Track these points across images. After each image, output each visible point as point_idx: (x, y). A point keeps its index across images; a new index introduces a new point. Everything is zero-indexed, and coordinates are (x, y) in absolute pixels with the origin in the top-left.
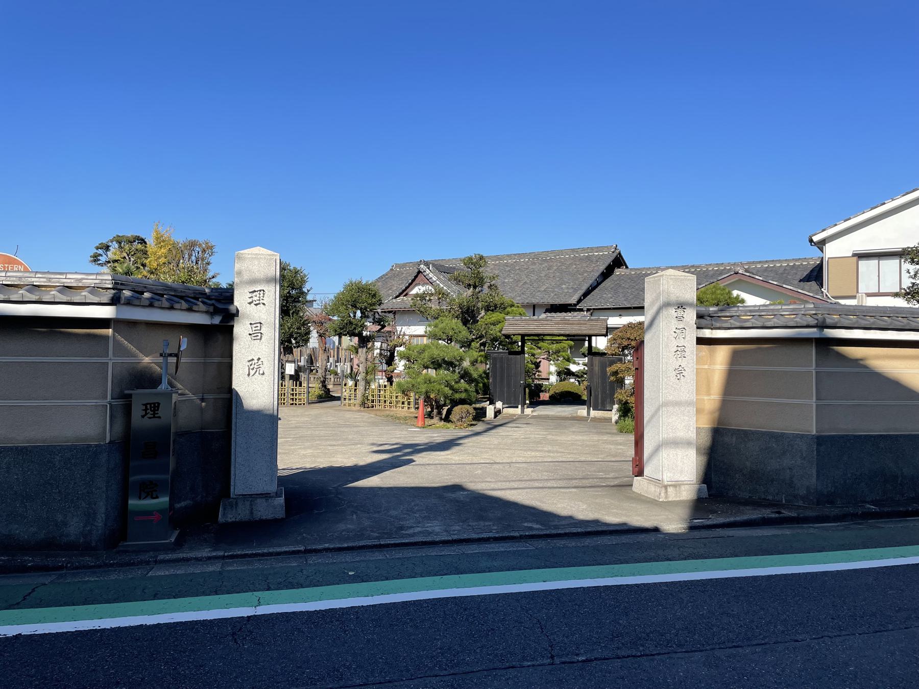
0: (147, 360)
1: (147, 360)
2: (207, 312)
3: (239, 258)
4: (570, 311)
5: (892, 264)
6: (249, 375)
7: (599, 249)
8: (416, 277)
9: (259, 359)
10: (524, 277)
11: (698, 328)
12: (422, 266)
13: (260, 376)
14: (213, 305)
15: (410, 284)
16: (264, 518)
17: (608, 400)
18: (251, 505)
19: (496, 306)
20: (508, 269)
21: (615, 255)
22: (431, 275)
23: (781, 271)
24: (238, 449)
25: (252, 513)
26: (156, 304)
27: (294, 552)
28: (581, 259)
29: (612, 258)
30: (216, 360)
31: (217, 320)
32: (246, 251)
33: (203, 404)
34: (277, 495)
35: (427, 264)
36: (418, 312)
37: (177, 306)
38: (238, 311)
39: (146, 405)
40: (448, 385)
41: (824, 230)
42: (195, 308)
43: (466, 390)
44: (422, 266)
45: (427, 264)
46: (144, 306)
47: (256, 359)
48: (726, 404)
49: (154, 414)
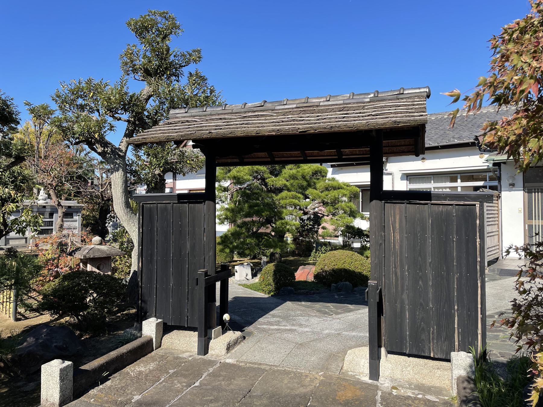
17: (433, 329)
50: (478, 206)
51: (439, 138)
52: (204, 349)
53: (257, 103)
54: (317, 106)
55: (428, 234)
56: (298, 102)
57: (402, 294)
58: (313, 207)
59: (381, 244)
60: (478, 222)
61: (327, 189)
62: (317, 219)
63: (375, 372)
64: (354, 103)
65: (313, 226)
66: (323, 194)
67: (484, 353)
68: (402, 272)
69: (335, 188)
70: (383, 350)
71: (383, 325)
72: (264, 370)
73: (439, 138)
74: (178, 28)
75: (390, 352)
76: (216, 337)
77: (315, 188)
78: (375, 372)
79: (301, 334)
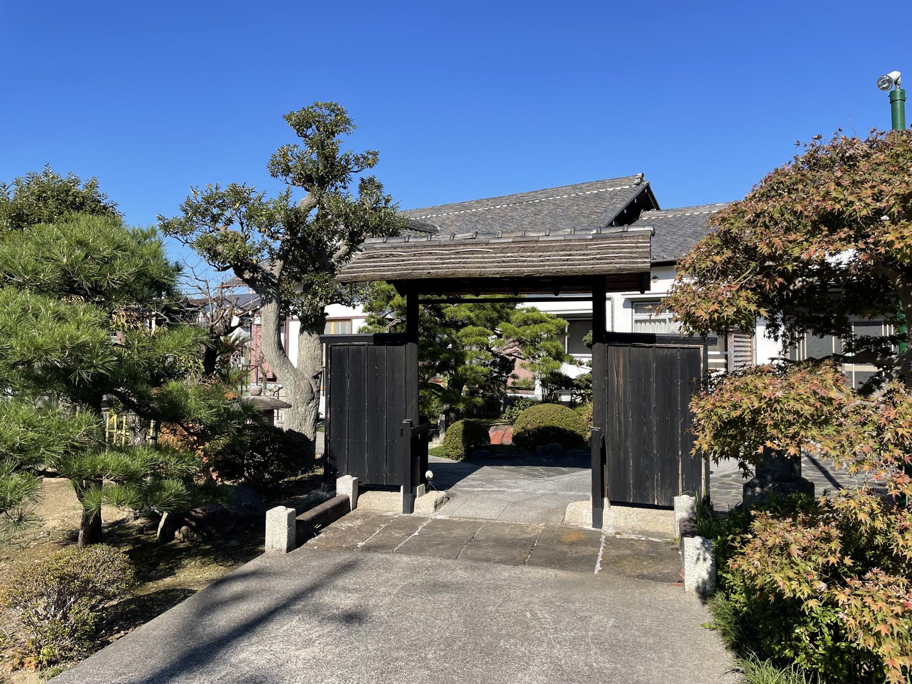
17: (658, 476)
20: (474, 219)
21: (641, 188)
28: (586, 198)
50: (702, 349)
51: (676, 248)
52: (409, 506)
53: (469, 235)
54: (536, 241)
55: (653, 376)
56: (514, 235)
57: (626, 441)
58: (508, 349)
59: (604, 390)
60: (702, 365)
61: (525, 323)
62: (506, 365)
63: (598, 520)
64: (576, 240)
65: (500, 373)
66: (521, 330)
67: (708, 497)
68: (626, 418)
69: (536, 322)
70: (606, 501)
71: (606, 474)
72: (481, 524)
73: (676, 248)
74: (347, 122)
75: (613, 503)
76: (421, 495)
77: (508, 321)
78: (598, 520)
79: (513, 494)
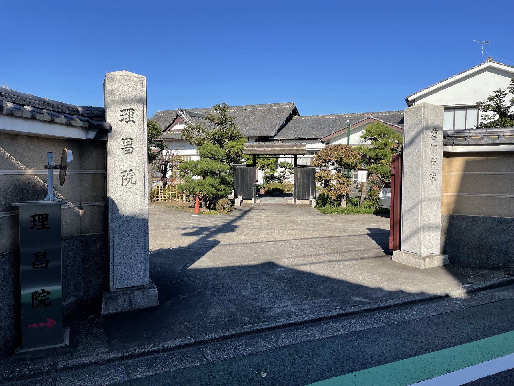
0: (29, 172)
1: (29, 172)
2: (82, 128)
3: (110, 79)
4: (270, 140)
5: (473, 113)
6: (122, 184)
7: (283, 104)
8: (176, 119)
9: (131, 170)
10: (241, 120)
11: (445, 145)
12: (179, 112)
13: (133, 186)
14: (87, 121)
15: (172, 123)
16: (141, 307)
18: (130, 297)
19: (235, 136)
21: (293, 107)
22: (185, 118)
23: (386, 118)
24: (116, 250)
25: (130, 304)
26: (38, 116)
27: (186, 346)
29: (292, 110)
30: (91, 172)
31: (91, 135)
32: (112, 73)
33: (81, 211)
34: (151, 287)
35: (182, 111)
36: (184, 141)
37: (57, 120)
38: (111, 127)
39: (34, 216)
40: (213, 186)
41: (414, 94)
42: (73, 123)
43: (224, 190)
44: (179, 112)
45: (182, 111)
46: (26, 118)
47: (128, 170)
48: (459, 199)
49: (43, 225)
